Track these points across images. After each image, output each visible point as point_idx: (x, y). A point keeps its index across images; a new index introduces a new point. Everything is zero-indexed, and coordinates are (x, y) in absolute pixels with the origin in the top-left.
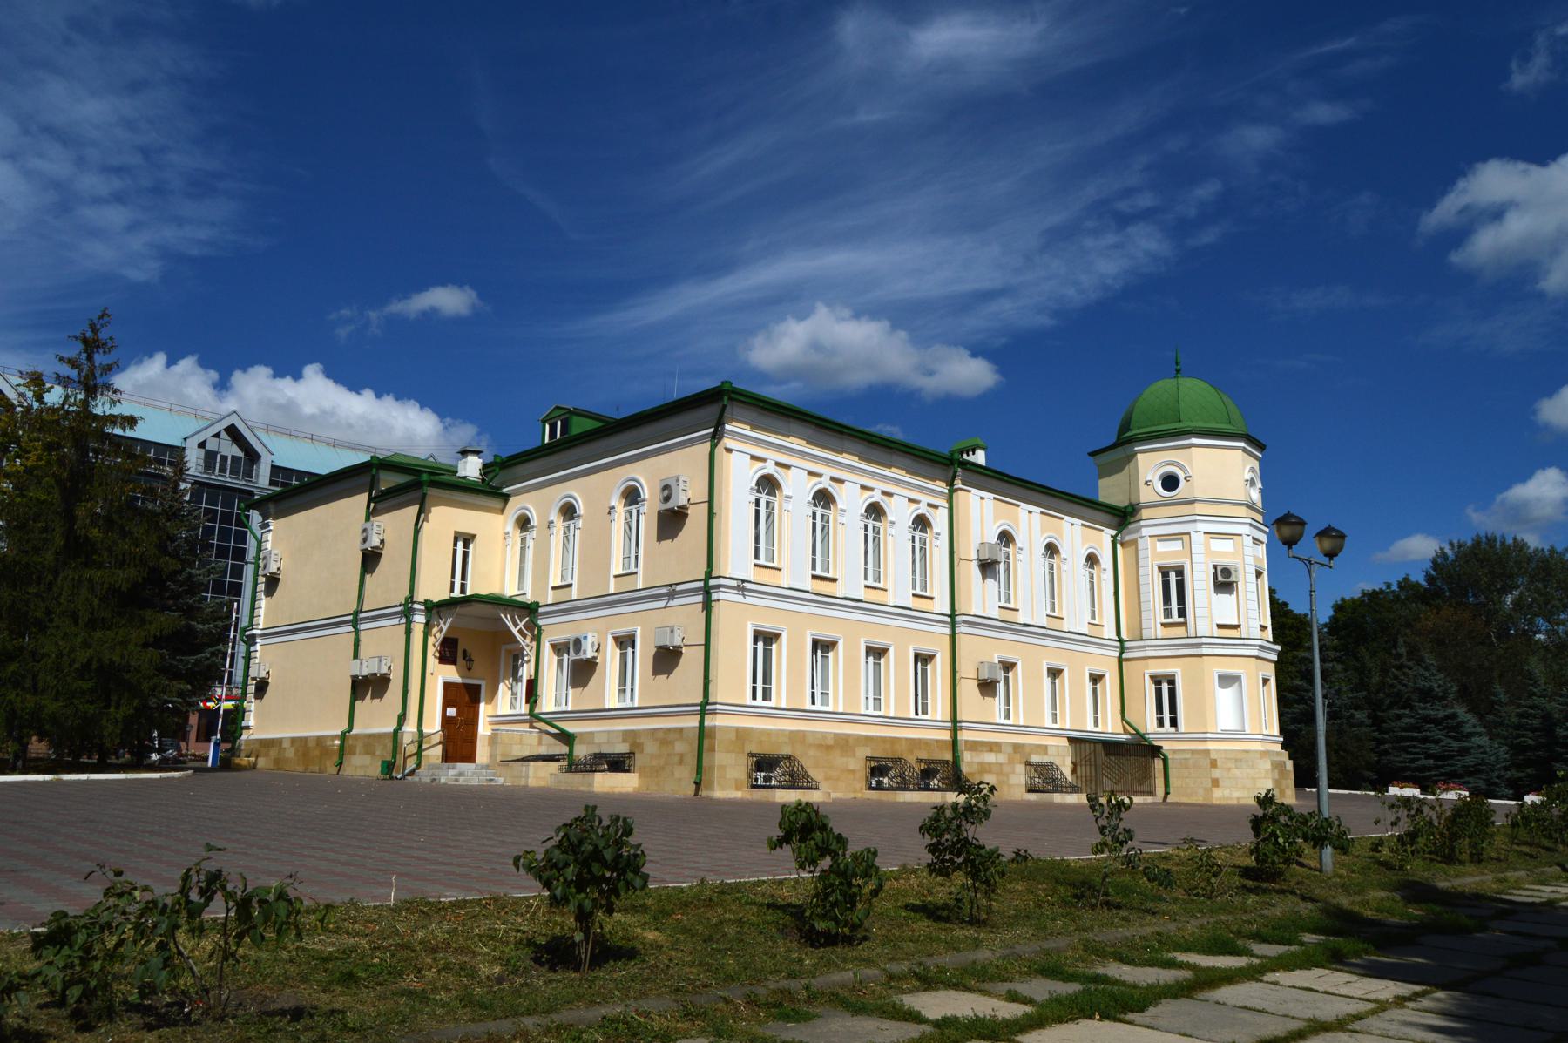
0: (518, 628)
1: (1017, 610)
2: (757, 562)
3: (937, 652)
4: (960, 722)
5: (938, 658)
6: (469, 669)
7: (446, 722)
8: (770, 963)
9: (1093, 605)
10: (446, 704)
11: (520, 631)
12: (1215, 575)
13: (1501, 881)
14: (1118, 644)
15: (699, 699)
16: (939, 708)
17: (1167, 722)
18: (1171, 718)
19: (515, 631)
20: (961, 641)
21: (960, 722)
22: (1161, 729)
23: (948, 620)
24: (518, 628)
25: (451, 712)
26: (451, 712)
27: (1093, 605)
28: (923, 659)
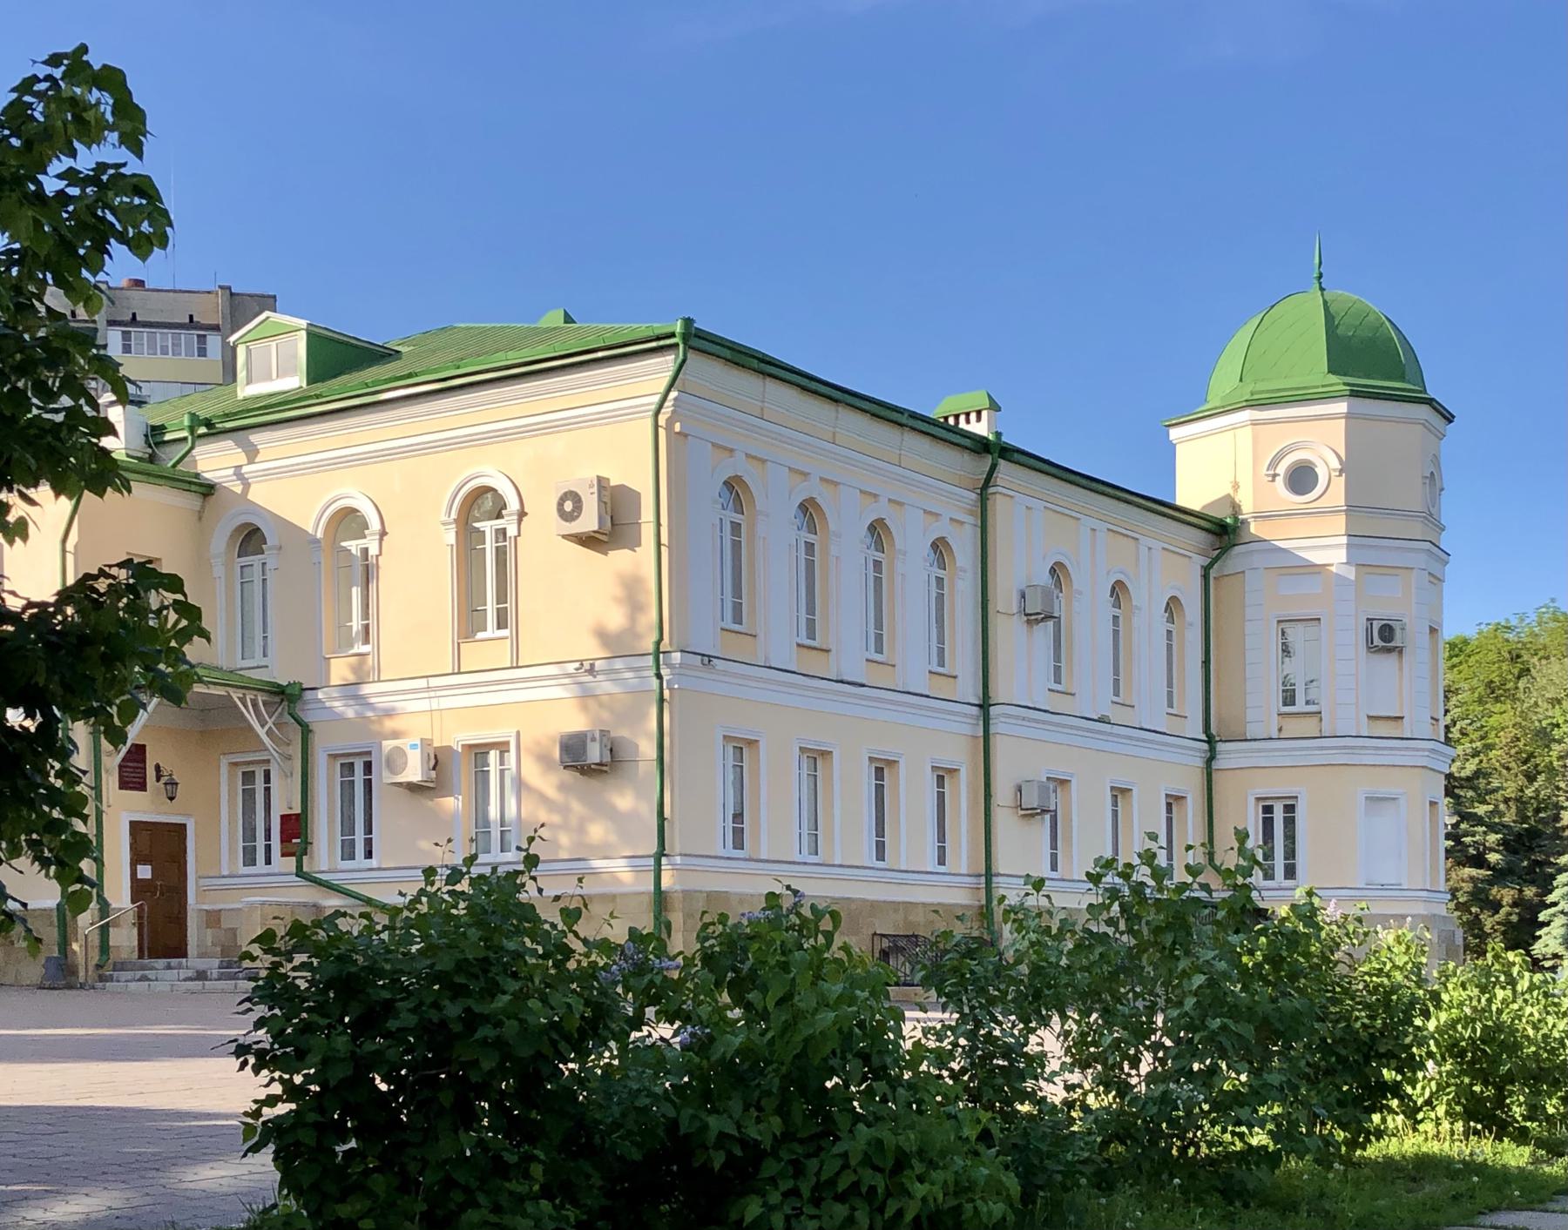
0: (267, 728)
1: (828, 651)
2: (1116, 699)
3: (1072, 775)
4: (999, 875)
5: (1189, 800)
6: (171, 799)
7: (139, 889)
8: (1531, 1032)
9: (1170, 685)
10: (135, 862)
11: (269, 733)
12: (1369, 631)
13: (1445, 1139)
14: (1205, 746)
15: (654, 849)
16: (964, 856)
17: (1279, 870)
18: (1286, 866)
19: (262, 732)
20: (999, 746)
21: (999, 875)
22: (349, 864)
23: (975, 710)
24: (267, 728)
25: (145, 872)
26: (145, 872)
27: (1170, 685)
28: (942, 777)
